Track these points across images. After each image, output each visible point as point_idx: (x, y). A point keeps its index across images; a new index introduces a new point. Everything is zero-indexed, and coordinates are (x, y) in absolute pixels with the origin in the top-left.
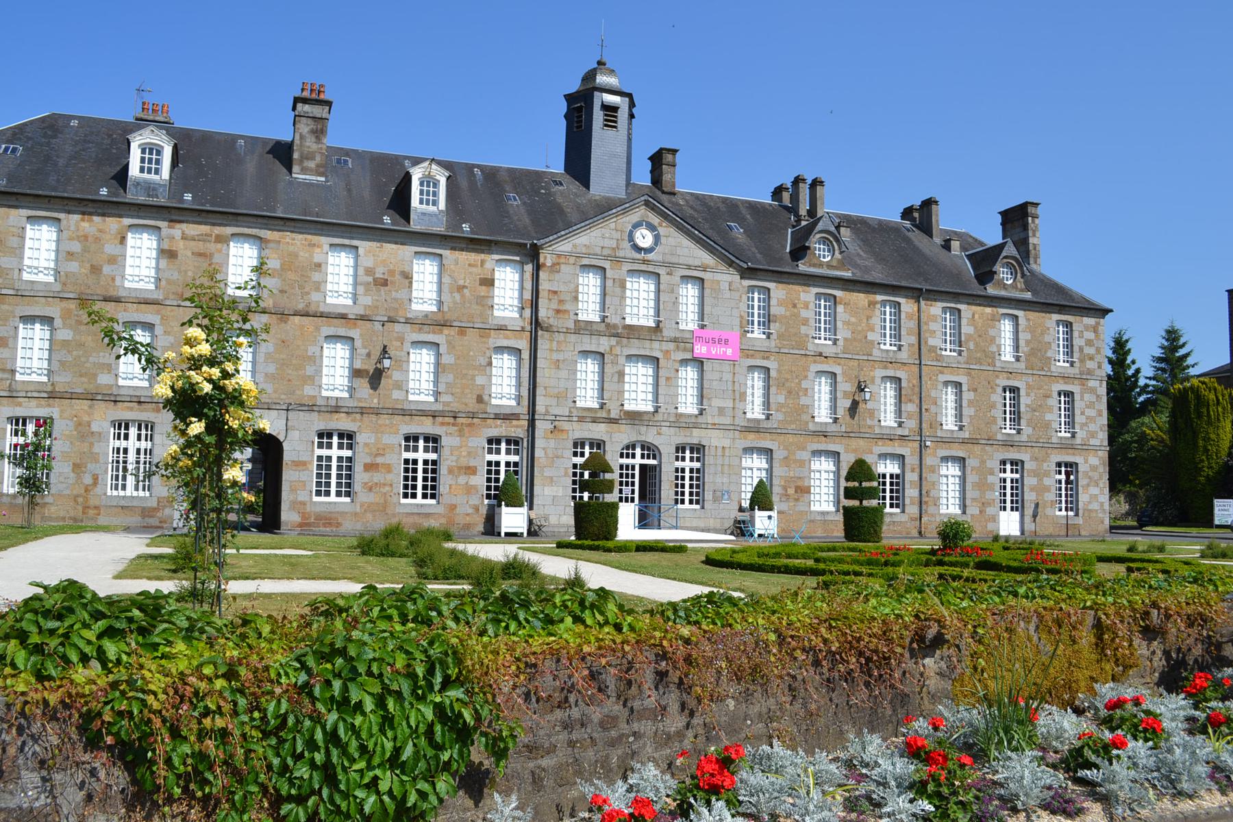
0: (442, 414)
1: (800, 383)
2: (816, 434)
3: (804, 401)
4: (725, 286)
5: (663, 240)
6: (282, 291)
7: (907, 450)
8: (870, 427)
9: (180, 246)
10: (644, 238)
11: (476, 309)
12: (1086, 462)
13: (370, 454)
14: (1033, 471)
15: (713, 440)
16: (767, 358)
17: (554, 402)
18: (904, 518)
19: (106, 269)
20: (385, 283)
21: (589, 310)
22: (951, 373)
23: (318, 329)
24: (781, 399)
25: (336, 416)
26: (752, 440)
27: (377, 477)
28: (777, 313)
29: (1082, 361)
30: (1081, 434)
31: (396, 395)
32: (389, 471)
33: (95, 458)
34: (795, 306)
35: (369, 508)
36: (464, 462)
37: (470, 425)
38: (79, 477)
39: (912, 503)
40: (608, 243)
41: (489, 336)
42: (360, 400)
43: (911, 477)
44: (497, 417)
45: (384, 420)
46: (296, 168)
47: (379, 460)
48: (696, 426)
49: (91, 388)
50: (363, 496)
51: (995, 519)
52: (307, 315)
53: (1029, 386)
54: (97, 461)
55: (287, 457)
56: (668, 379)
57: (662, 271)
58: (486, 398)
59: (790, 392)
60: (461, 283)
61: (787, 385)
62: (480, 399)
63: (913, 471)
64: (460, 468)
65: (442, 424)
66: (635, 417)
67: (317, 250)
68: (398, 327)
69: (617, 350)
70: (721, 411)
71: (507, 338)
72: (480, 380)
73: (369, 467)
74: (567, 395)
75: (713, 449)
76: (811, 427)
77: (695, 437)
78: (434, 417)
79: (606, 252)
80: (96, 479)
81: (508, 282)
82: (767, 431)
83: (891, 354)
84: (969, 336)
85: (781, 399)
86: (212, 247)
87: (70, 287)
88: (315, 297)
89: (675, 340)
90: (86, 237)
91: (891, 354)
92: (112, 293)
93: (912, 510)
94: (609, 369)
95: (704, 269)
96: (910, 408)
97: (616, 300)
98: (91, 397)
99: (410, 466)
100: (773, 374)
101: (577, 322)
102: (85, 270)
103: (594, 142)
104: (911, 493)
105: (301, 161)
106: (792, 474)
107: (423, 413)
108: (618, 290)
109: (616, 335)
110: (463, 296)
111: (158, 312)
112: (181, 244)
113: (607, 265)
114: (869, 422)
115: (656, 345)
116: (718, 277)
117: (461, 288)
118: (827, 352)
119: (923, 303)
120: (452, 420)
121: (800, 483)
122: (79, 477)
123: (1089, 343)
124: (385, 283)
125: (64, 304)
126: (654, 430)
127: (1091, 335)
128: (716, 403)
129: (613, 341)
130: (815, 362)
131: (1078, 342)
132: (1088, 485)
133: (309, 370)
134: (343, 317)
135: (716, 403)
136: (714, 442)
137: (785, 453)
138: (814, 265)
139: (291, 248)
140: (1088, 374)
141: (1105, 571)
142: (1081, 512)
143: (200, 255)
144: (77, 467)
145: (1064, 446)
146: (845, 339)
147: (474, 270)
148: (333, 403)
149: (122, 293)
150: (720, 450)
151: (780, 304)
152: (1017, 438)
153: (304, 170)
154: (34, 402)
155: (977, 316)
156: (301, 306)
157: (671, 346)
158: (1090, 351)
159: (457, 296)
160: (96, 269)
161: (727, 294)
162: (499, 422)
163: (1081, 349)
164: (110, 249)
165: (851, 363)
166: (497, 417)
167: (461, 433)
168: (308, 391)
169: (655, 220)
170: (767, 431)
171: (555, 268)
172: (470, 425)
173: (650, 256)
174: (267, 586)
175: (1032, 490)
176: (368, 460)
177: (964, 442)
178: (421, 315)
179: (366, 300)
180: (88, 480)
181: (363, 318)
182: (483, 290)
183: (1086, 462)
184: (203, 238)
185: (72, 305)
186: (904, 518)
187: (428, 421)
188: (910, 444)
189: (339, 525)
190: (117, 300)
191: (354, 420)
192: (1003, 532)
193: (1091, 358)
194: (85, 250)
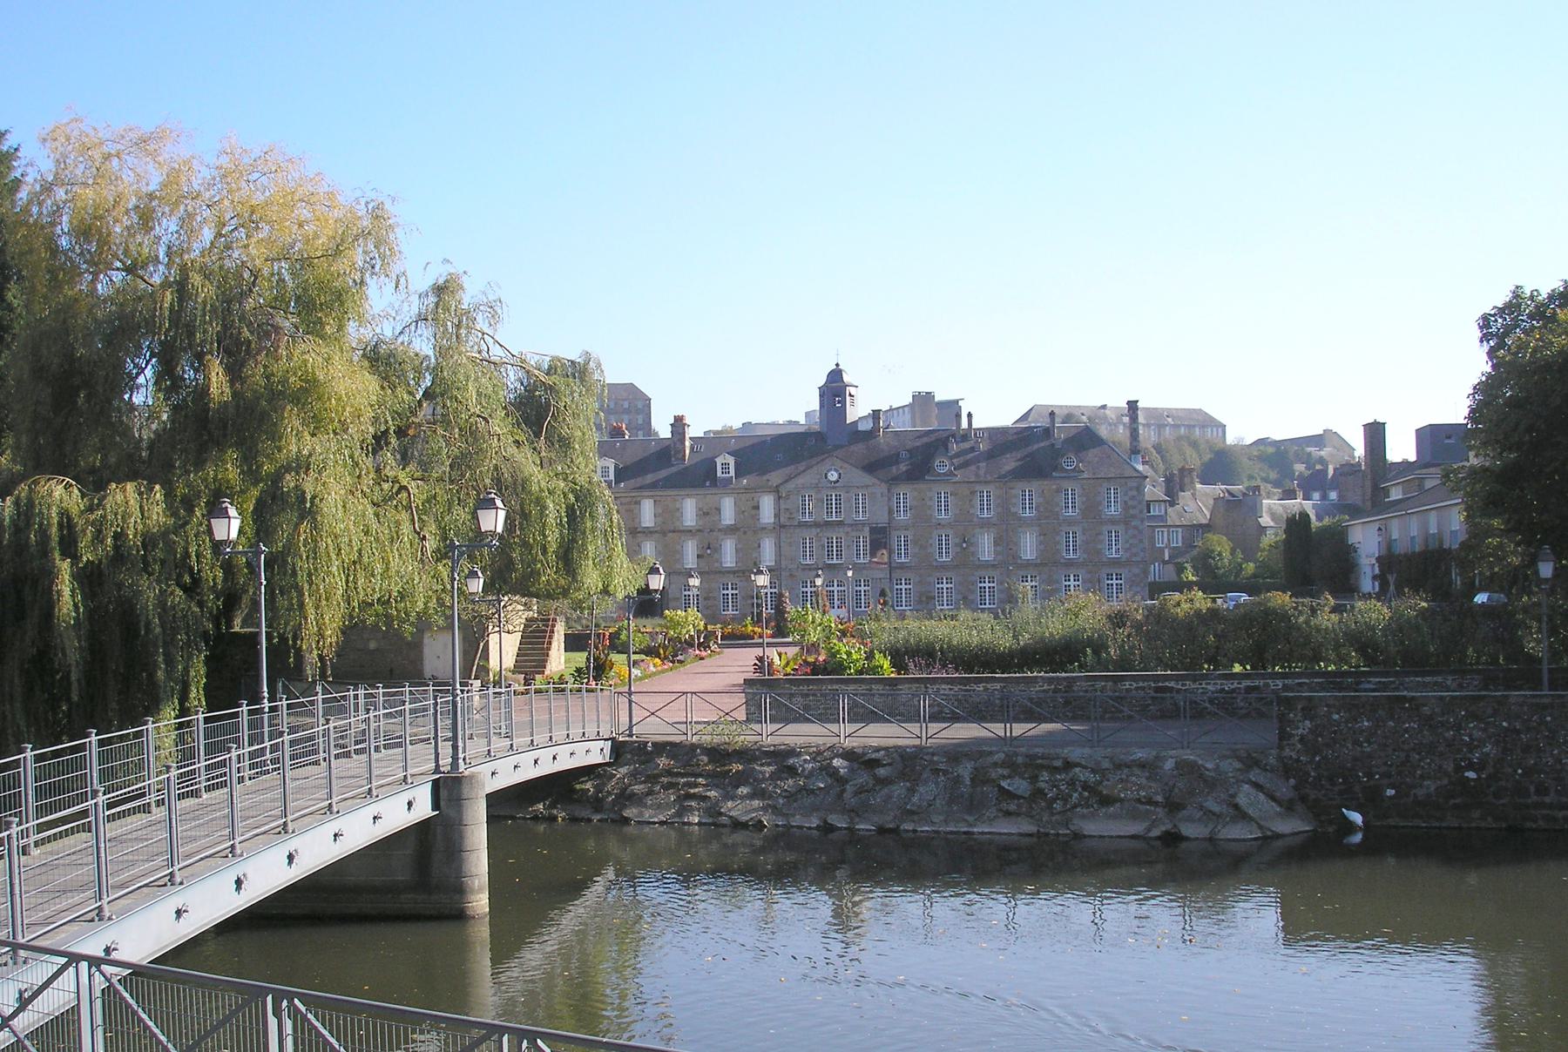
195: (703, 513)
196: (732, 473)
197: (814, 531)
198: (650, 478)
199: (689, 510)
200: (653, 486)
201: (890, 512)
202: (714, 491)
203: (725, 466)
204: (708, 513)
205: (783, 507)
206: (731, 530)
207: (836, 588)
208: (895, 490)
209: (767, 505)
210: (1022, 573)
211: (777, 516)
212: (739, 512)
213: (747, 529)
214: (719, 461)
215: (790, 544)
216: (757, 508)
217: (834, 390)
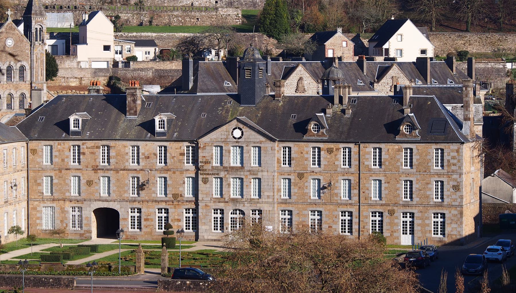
0: (168, 201)
1: (304, 184)
2: (310, 204)
3: (306, 191)
5: (244, 133)
6: (117, 163)
7: (354, 210)
8: (336, 200)
10: (237, 133)
11: (178, 164)
12: (450, 212)
13: (146, 215)
14: (419, 217)
15: (265, 208)
16: (290, 175)
17: (205, 196)
18: (352, 237)
19: (66, 160)
20: (148, 158)
22: (376, 176)
23: (128, 175)
24: (296, 190)
25: (135, 203)
26: (284, 207)
27: (148, 223)
28: (294, 157)
29: (449, 166)
30: (446, 200)
31: (153, 195)
32: (152, 221)
33: (66, 218)
34: (302, 153)
35: (146, 233)
36: (176, 217)
37: (178, 205)
38: (62, 225)
39: (356, 231)
40: (223, 137)
41: (183, 173)
42: (142, 198)
43: (355, 220)
44: (187, 201)
45: (150, 204)
46: (127, 114)
47: (149, 217)
48: (258, 203)
49: (64, 197)
50: (144, 229)
51: (398, 238)
52: (124, 170)
53: (417, 180)
54: (67, 219)
55: (121, 217)
56: (247, 186)
57: (244, 146)
58: (183, 195)
59: (300, 188)
60: (173, 155)
61: (299, 185)
63: (356, 218)
64: (175, 219)
65: (169, 205)
66: (234, 200)
67: (127, 148)
68: (153, 172)
69: (227, 176)
70: (268, 197)
71: (190, 174)
72: (181, 189)
73: (146, 220)
74: (209, 193)
75: (265, 211)
76: (309, 201)
77: (258, 206)
78: (166, 202)
79: (222, 140)
80: (67, 225)
82: (289, 203)
83: (346, 170)
84: (386, 160)
85: (296, 190)
87: (56, 167)
89: (249, 171)
90: (60, 150)
91: (346, 170)
92: (68, 167)
93: (355, 234)
94: (224, 183)
95: (261, 142)
96: (355, 192)
97: (227, 158)
99: (374, 221)
100: (292, 181)
101: (212, 167)
102: (60, 161)
104: (355, 227)
105: (129, 111)
106: (301, 220)
107: (162, 201)
108: (227, 154)
109: (227, 171)
110: (174, 160)
111: (81, 172)
112: (86, 150)
113: (223, 145)
114: (335, 198)
115: (242, 173)
116: (267, 145)
117: (173, 157)
118: (316, 170)
119: (362, 145)
120: (172, 203)
121: (304, 224)
122: (62, 225)
123: (454, 158)
124: (148, 158)
125: (55, 172)
126: (242, 205)
127: (455, 154)
128: (266, 194)
129: (226, 173)
130: (311, 175)
131: (446, 158)
132: (451, 223)
134: (135, 170)
135: (266, 194)
136: (266, 209)
137: (298, 212)
138: (311, 136)
139: (118, 148)
140: (452, 172)
142: (446, 235)
143: (92, 153)
144: (62, 221)
145: (437, 205)
146: (325, 165)
147: (177, 150)
148: (134, 199)
149: (71, 167)
150: (268, 212)
151: (296, 153)
152: (411, 203)
153: (130, 114)
154: (49, 202)
155: (390, 150)
156: (123, 167)
157: (248, 173)
158: (452, 161)
159: (172, 160)
160: (63, 160)
161: (271, 152)
162: (187, 203)
163: (448, 161)
165: (327, 175)
166: (187, 201)
167: (175, 208)
169: (241, 126)
170: (289, 203)
171: (204, 148)
172: (178, 205)
173: (239, 140)
174: (6, 222)
175: (418, 225)
176: (145, 218)
177: (382, 205)
178: (160, 168)
180: (65, 225)
181: (142, 170)
183: (450, 212)
184: (92, 147)
185: (57, 172)
186: (352, 237)
187: (164, 204)
188: (355, 207)
189: (137, 239)
191: (141, 204)
193: (454, 165)
194: (60, 155)
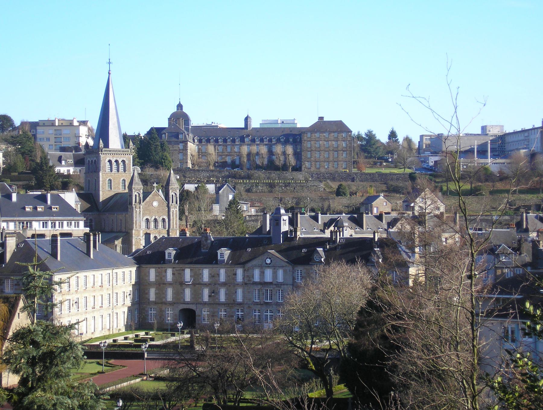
4: (288, 271)
9: (175, 272)
19: (163, 278)
20: (214, 276)
21: (257, 278)
31: (217, 300)
40: (259, 263)
62: (234, 301)
72: (234, 296)
81: (240, 272)
86: (181, 272)
88: (200, 281)
98: (162, 303)
103: (121, 360)
124: (214, 276)
133: (200, 296)
141: (467, 237)
153: (204, 249)
160: (161, 278)
164: (164, 274)
168: (200, 300)
179: (211, 280)
182: (234, 276)
190: (165, 284)
192: (410, 269)
195: (211, 276)
196: (172, 258)
197: (260, 287)
198: (351, 249)
199: (206, 274)
200: (191, 263)
201: (294, 279)
202: (216, 266)
203: (170, 254)
204: (161, 276)
205: (246, 274)
206: (224, 284)
207: (269, 314)
208: (296, 268)
209: (188, 273)
210: (237, 308)
211: (243, 279)
212: (227, 276)
213: (230, 284)
214: (167, 252)
215: (249, 292)
216: (235, 274)
217: (534, 126)
